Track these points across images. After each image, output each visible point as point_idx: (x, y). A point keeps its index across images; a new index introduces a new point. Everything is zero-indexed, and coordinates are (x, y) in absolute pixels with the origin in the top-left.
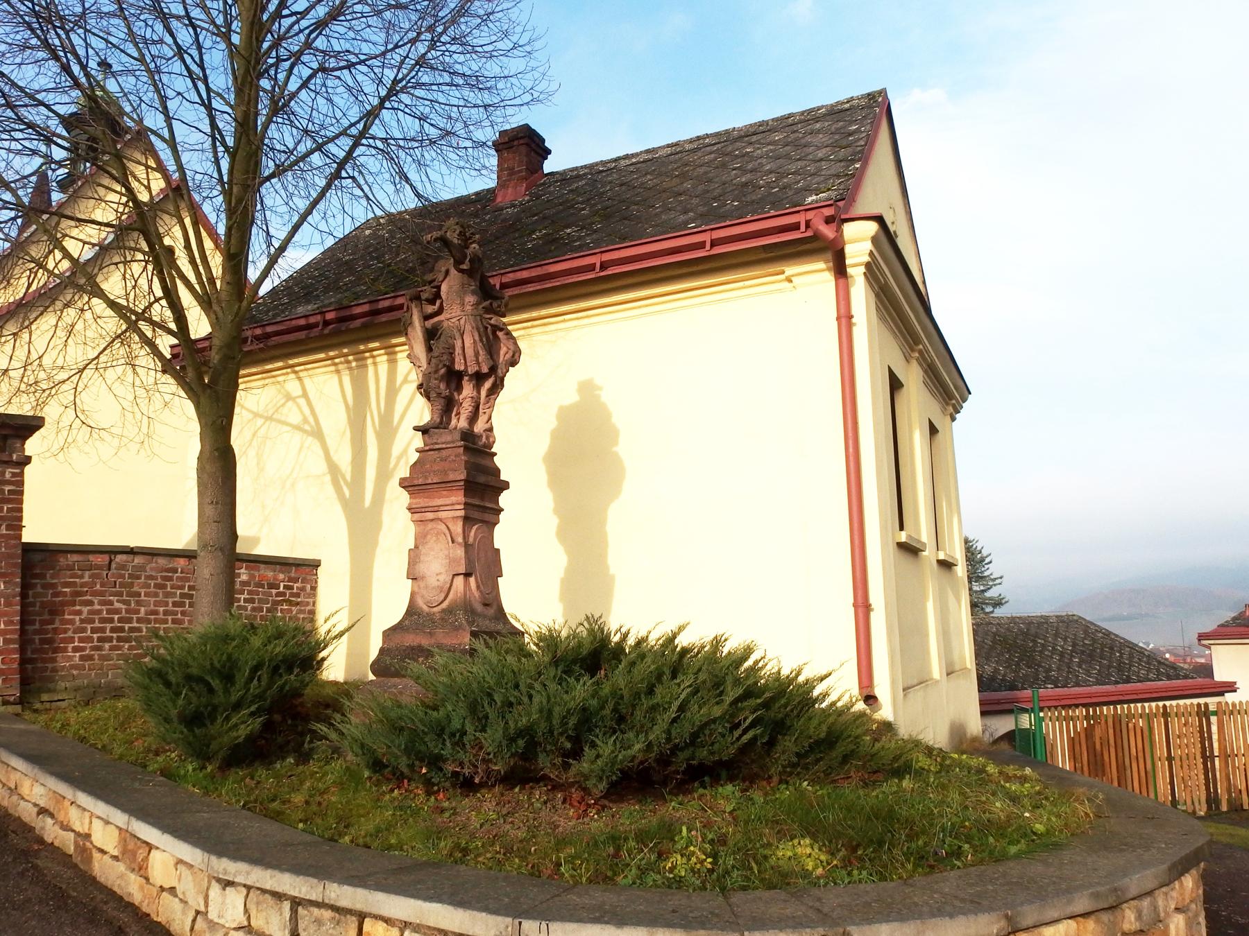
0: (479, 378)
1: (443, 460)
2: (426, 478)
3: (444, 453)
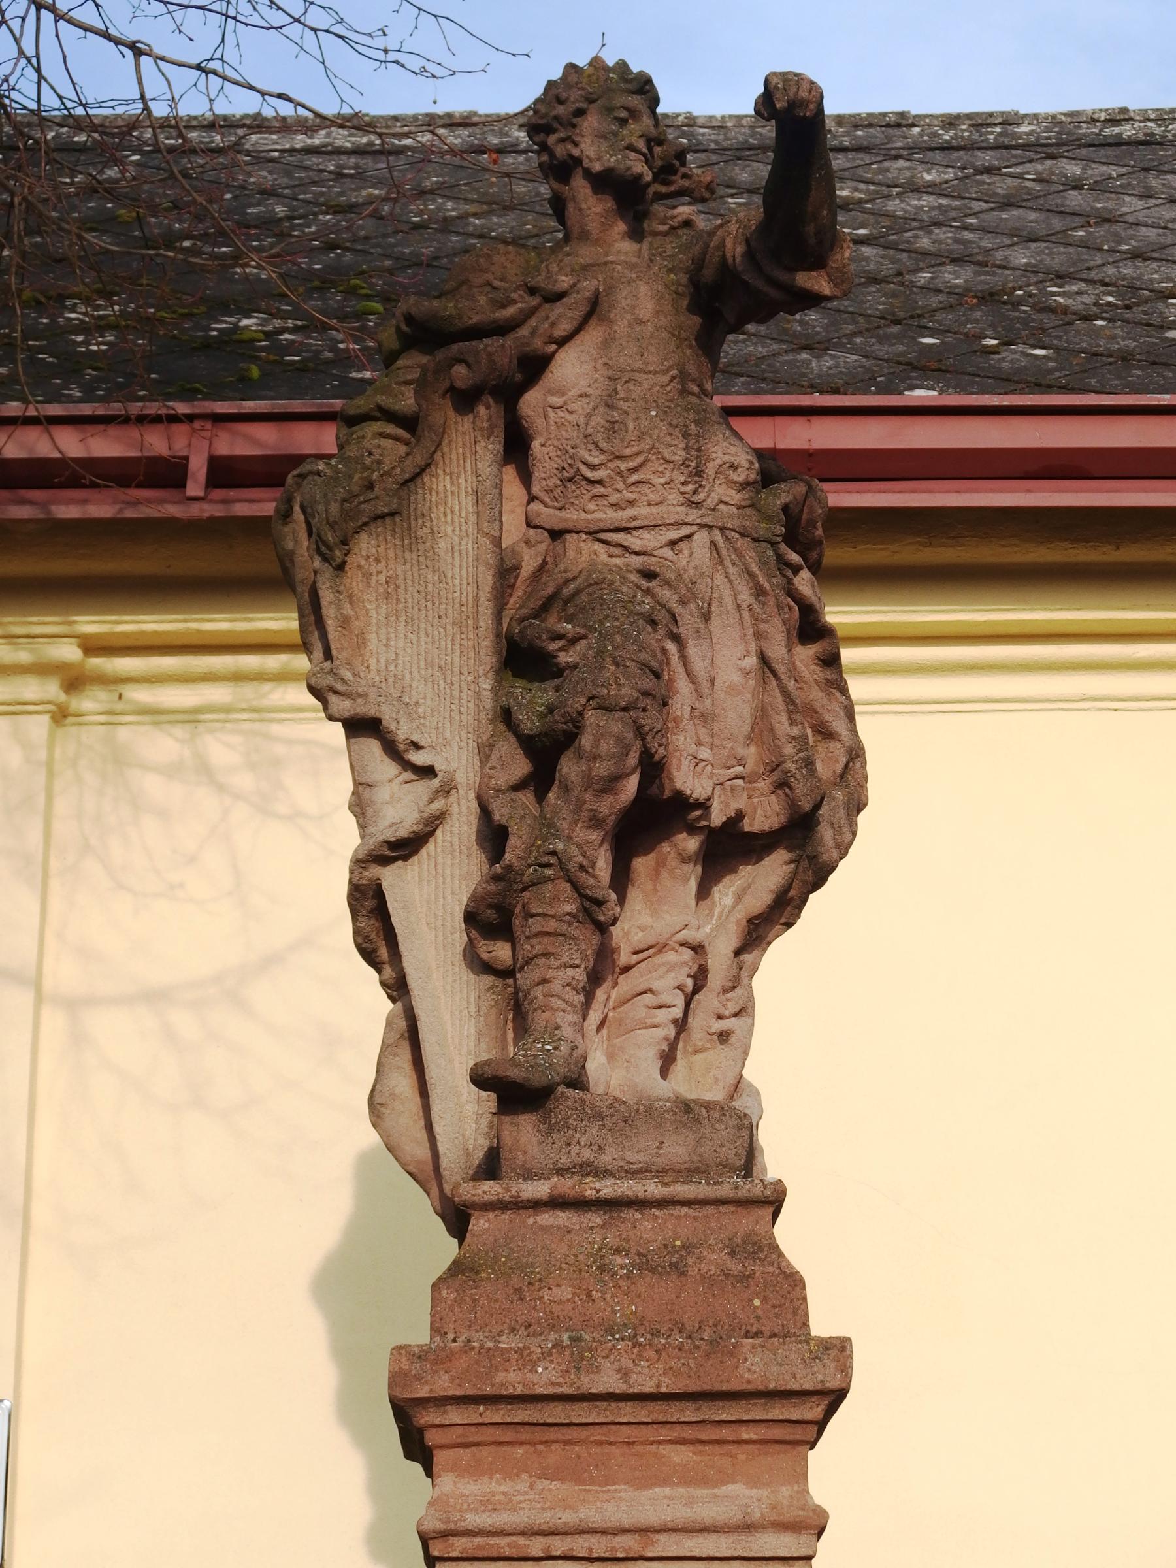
0: (727, 848)
1: (673, 1264)
2: (580, 1356)
3: (647, 1229)
